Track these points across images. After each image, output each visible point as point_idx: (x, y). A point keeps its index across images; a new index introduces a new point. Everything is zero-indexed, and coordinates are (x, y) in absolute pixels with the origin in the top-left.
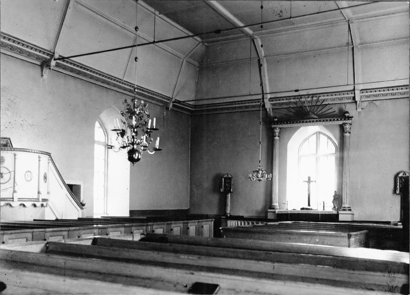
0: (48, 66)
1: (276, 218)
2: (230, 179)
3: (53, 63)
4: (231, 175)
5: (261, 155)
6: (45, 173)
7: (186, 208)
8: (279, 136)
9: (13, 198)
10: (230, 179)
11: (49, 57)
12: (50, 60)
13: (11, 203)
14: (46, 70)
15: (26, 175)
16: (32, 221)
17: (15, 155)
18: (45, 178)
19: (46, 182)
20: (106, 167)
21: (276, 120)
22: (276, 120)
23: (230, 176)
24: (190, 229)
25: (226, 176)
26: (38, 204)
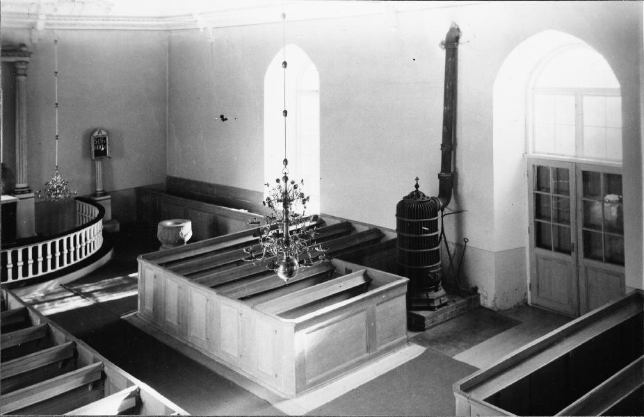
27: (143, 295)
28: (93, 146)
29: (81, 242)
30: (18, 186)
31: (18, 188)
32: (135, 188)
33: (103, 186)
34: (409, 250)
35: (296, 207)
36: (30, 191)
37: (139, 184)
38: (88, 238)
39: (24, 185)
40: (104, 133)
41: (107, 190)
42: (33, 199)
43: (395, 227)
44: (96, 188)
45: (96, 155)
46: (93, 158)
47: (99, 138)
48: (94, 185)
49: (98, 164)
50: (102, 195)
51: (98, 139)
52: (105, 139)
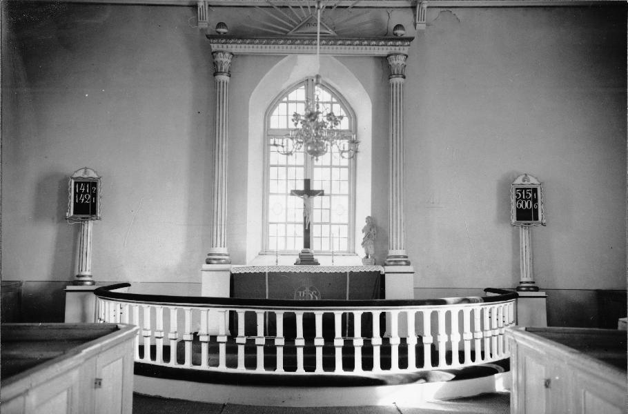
2: (93, 184)
4: (95, 172)
10: (93, 184)
27: (523, 388)
28: (513, 201)
29: (473, 330)
30: (392, 253)
31: (391, 257)
32: (597, 290)
33: (533, 274)
34: (319, 32)
35: (347, 149)
36: (408, 264)
37: (602, 286)
38: (487, 326)
39: (401, 252)
40: (533, 180)
41: (539, 284)
42: (544, 299)
43: (272, 154)
44: (520, 278)
45: (519, 218)
46: (514, 220)
47: (525, 189)
48: (517, 270)
49: (524, 234)
50: (528, 289)
51: (522, 189)
52: (535, 190)
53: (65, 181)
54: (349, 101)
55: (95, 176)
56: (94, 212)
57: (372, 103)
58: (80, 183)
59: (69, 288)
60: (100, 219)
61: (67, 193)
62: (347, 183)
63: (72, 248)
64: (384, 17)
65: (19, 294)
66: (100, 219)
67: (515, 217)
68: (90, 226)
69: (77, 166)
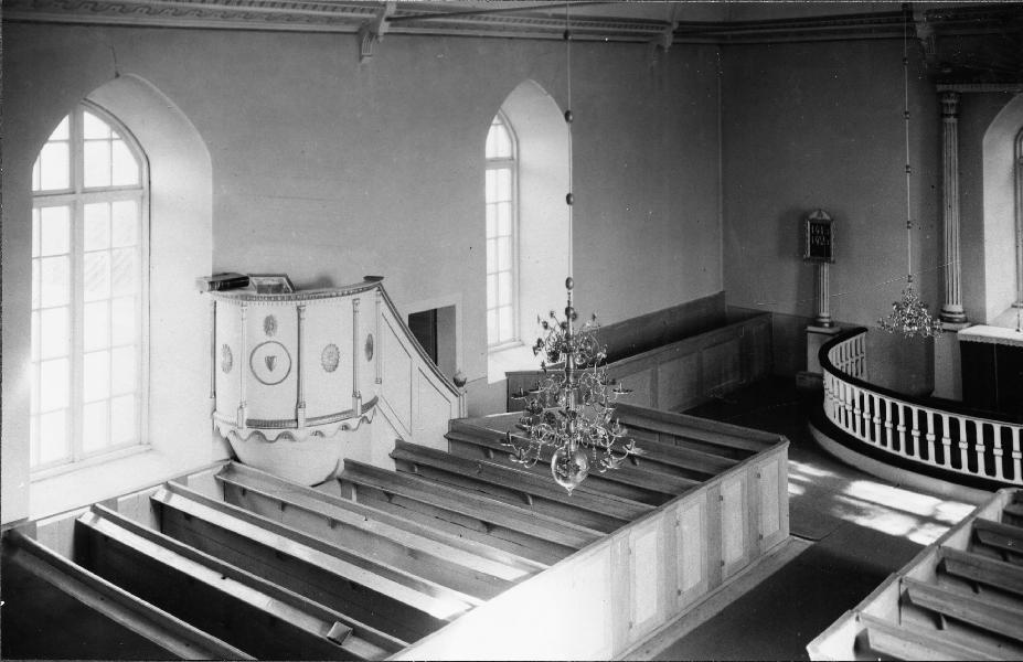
0: (373, 35)
1: (959, 398)
2: (826, 226)
3: (384, 27)
4: (828, 214)
5: (909, 188)
6: (370, 336)
7: (716, 292)
8: (956, 116)
9: (297, 420)
10: (826, 226)
11: (374, 16)
12: (376, 23)
13: (294, 432)
14: (371, 48)
15: (329, 350)
16: (363, 280)
17: (299, 309)
18: (370, 348)
19: (370, 359)
20: (515, 184)
21: (948, 71)
22: (948, 71)
23: (826, 217)
24: (726, 498)
25: (814, 215)
26: (353, 423)
53: (804, 216)
54: (876, 474)
55: (828, 218)
56: (828, 254)
57: (38, 153)
58: (815, 225)
59: (810, 328)
60: (834, 262)
61: (805, 238)
62: (487, 201)
63: (811, 289)
64: (338, 497)
65: (770, 327)
66: (834, 262)
67: (788, 530)
68: (826, 269)
69: (817, 197)
